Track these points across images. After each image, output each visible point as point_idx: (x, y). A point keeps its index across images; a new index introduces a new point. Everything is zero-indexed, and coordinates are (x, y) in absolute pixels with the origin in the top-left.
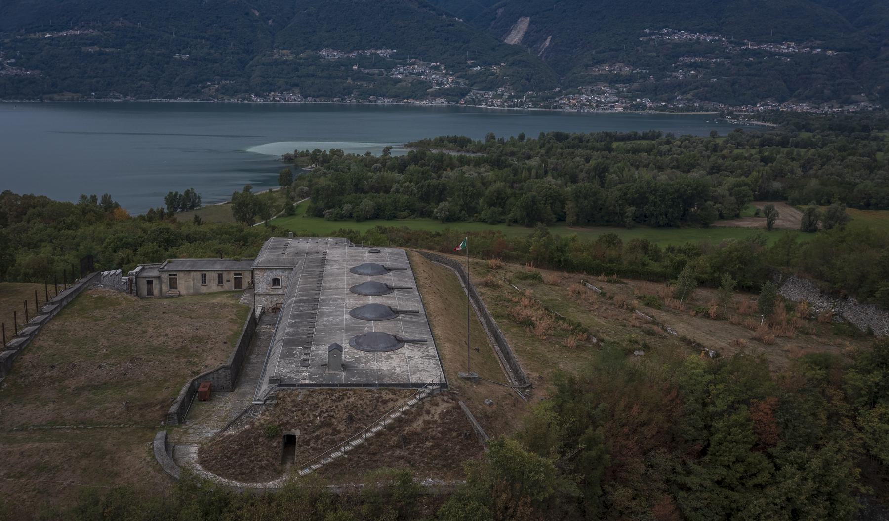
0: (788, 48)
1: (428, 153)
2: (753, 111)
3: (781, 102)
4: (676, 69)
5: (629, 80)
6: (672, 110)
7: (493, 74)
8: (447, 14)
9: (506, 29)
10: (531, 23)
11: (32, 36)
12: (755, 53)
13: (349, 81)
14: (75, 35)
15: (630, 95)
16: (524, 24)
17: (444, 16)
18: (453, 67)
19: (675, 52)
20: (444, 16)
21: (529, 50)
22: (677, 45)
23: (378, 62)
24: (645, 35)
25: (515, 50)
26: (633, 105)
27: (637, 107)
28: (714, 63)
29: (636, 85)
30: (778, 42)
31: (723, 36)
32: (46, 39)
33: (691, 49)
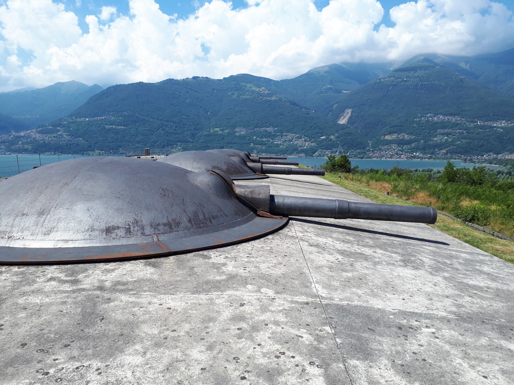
0: (501, 123)
1: (313, 339)
2: (482, 159)
3: (498, 154)
4: (436, 136)
5: (409, 142)
6: (435, 159)
7: (331, 140)
8: (306, 108)
9: (338, 117)
10: (352, 112)
11: (79, 120)
12: (481, 127)
13: (252, 145)
14: (102, 119)
15: (410, 151)
16: (348, 113)
17: (304, 109)
18: (311, 137)
19: (434, 127)
20: (304, 109)
21: (351, 127)
22: (436, 123)
23: (269, 135)
24: (418, 117)
25: (343, 127)
26: (412, 157)
27: (414, 157)
28: (458, 132)
29: (413, 145)
30: (496, 120)
31: (463, 118)
32: (86, 121)
33: (444, 125)
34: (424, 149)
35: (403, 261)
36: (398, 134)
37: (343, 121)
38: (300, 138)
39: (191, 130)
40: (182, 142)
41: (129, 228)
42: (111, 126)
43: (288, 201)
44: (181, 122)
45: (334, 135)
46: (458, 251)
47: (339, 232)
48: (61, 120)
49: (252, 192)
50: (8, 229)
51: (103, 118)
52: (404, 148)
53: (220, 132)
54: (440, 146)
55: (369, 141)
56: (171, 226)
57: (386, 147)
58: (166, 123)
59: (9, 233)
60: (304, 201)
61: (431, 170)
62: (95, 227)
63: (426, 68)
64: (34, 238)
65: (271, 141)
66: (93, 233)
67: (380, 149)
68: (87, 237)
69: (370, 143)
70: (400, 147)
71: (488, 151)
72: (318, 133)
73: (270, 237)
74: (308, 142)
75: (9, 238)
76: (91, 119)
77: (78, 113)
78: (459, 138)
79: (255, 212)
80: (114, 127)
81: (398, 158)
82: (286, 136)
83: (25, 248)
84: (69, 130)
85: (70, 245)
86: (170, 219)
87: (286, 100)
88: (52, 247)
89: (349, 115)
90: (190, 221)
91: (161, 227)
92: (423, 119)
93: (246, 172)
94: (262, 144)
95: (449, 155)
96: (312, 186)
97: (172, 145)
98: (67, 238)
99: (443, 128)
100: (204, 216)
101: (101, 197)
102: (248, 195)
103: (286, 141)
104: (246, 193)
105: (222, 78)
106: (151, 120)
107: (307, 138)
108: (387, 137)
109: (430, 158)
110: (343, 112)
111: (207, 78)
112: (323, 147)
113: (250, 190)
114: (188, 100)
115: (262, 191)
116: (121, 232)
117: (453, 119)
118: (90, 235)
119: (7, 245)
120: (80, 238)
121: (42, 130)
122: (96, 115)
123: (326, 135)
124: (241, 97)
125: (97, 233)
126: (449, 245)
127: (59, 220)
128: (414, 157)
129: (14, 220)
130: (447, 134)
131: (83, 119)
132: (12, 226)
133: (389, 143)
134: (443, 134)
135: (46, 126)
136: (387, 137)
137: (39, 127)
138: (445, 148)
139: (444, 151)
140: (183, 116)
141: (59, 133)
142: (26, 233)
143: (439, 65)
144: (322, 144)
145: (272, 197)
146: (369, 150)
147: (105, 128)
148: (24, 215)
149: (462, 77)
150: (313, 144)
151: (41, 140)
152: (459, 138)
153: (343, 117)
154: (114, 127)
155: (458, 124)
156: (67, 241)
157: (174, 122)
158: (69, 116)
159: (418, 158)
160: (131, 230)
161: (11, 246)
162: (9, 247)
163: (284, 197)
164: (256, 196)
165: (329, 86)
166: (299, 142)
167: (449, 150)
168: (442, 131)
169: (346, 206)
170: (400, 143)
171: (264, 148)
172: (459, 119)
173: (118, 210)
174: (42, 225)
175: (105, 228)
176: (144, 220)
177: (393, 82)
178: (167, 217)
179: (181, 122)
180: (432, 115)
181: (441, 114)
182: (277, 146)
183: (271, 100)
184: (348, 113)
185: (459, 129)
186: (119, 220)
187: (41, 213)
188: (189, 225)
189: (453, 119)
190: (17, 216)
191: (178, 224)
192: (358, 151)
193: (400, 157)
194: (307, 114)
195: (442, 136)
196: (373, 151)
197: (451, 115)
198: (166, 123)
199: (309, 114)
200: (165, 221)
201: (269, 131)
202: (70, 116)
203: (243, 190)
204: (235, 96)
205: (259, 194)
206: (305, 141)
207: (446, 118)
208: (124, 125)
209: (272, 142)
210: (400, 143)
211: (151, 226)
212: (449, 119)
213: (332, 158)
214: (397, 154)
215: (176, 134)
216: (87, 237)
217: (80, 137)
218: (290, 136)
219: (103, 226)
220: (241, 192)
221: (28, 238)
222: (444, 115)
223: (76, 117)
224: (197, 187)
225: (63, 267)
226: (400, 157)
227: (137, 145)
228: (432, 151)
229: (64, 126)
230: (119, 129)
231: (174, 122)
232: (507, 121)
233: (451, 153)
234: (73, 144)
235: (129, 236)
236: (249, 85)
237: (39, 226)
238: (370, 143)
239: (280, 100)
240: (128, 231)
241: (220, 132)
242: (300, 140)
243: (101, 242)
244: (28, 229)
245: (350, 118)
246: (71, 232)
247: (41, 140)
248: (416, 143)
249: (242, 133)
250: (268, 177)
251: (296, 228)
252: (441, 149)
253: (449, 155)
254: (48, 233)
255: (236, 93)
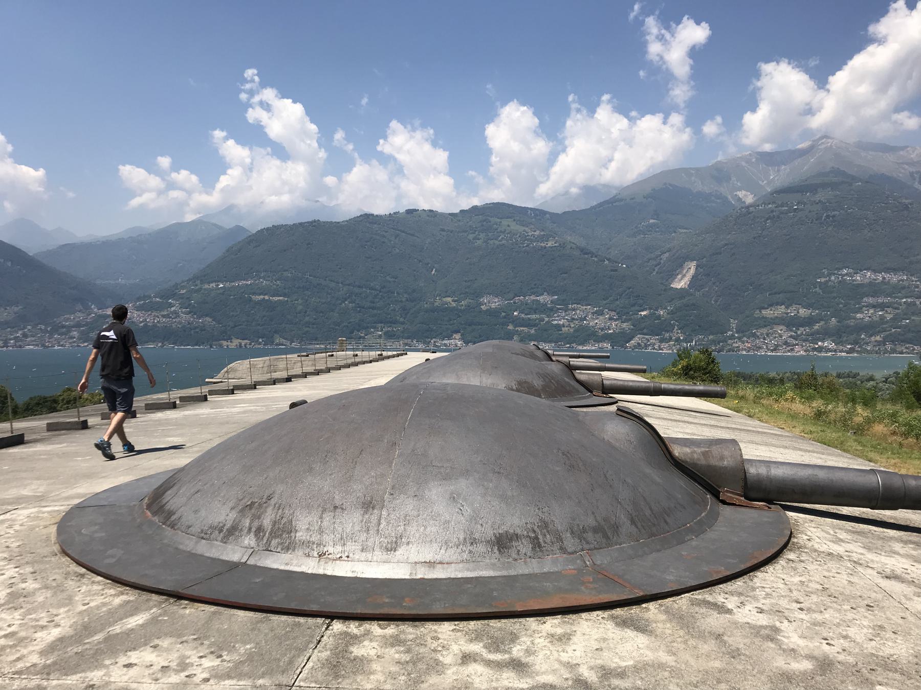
4: (860, 310)
7: (659, 317)
9: (672, 274)
10: (697, 267)
11: (206, 286)
13: (511, 327)
16: (691, 268)
18: (622, 315)
19: (857, 292)
20: (606, 262)
24: (823, 276)
25: (682, 293)
28: (905, 303)
29: (816, 327)
33: (874, 289)
34: (838, 335)
36: (787, 308)
37: (680, 284)
38: (600, 313)
39: (401, 301)
40: (384, 323)
41: (537, 538)
42: (262, 297)
44: (384, 287)
45: (666, 308)
48: (176, 286)
49: (705, 454)
50: (315, 538)
51: (249, 283)
52: (799, 332)
53: (454, 304)
54: (871, 328)
55: (732, 320)
56: (606, 533)
57: (764, 331)
58: (356, 290)
59: (319, 545)
60: (809, 472)
61: (855, 375)
62: (477, 536)
63: (833, 186)
64: (369, 556)
65: (547, 319)
66: (473, 548)
67: (754, 335)
68: (465, 556)
69: (734, 323)
70: (792, 331)
72: (634, 305)
74: (616, 320)
75: (320, 556)
76: (228, 284)
77: (205, 276)
78: (905, 314)
79: (716, 494)
80: (267, 297)
81: (789, 351)
82: (574, 310)
83: (356, 578)
84: (190, 305)
85: (439, 573)
86: (599, 519)
87: (574, 246)
88: (407, 577)
89: (692, 271)
90: (633, 522)
91: (590, 536)
92: (833, 278)
93: (578, 392)
94: (529, 324)
95: (889, 346)
97: (368, 327)
98: (429, 557)
99: (875, 294)
100: (651, 509)
101: (466, 473)
102: (698, 459)
103: (574, 319)
104: (695, 456)
105: (458, 211)
106: (333, 285)
107: (613, 313)
108: (768, 313)
110: (681, 266)
111: (431, 211)
112: (645, 331)
113: (703, 449)
114: (398, 251)
115: (726, 453)
116: (525, 547)
117: (894, 278)
118: (470, 552)
119: (321, 572)
120: (454, 558)
121: (144, 304)
122: (237, 278)
123: (650, 309)
124: (491, 242)
125: (481, 548)
127: (407, 521)
128: (820, 349)
129: (321, 518)
130: (882, 306)
131: (213, 285)
132: (321, 531)
133: (769, 323)
134: (874, 306)
135: (149, 297)
136: (768, 313)
137: (139, 299)
138: (879, 332)
139: (878, 338)
140: (388, 278)
141: (173, 309)
142: (350, 546)
143: (860, 180)
144: (643, 325)
146: (732, 337)
147: (250, 300)
148: (336, 507)
149: (907, 201)
150: (624, 325)
151: (141, 322)
152: (905, 314)
153: (679, 276)
154: (267, 297)
155: (904, 288)
156: (431, 564)
157: (372, 289)
158: (189, 280)
160: (541, 541)
161: (329, 573)
162: (325, 576)
163: (768, 463)
164: (714, 462)
165: (651, 221)
166: (596, 322)
167: (887, 336)
168: (871, 300)
170: (792, 323)
171: (533, 331)
172: (905, 278)
173: (503, 498)
174: (378, 530)
175: (493, 538)
176: (556, 521)
177: (772, 211)
178: (593, 513)
179: (384, 287)
180: (851, 271)
181: (868, 269)
182: (559, 327)
183: (545, 247)
185: (906, 297)
186: (515, 521)
187: (368, 505)
188: (633, 529)
190: (324, 510)
191: (616, 528)
192: (711, 337)
193: (792, 350)
194: (612, 270)
195: (871, 311)
196: (740, 338)
197: (888, 270)
198: (356, 290)
199: (616, 270)
200: (591, 521)
201: (542, 301)
202: (195, 279)
203: (688, 450)
205: (722, 458)
206: (611, 319)
207: (880, 277)
208: (285, 295)
209: (548, 322)
210: (792, 323)
211: (572, 533)
212: (884, 278)
213: (684, 354)
214: (786, 343)
215: (373, 308)
216: (465, 556)
217: (207, 316)
218: (580, 311)
219: (490, 534)
220: (685, 454)
221: (357, 557)
222: (875, 271)
223: (202, 282)
224: (609, 444)
225: (462, 624)
226: (792, 350)
227: (307, 329)
228: (853, 337)
229: (181, 297)
230: (276, 302)
231: (372, 289)
233: (893, 341)
234: (196, 328)
235: (540, 554)
236: (505, 222)
237: (371, 532)
238: (734, 323)
239: (563, 246)
240: (536, 545)
241: (454, 304)
242: (601, 318)
243: (493, 566)
244: (352, 538)
245: (694, 277)
246: (435, 546)
247: (141, 322)
248: (822, 323)
249: (493, 305)
252: (871, 336)
253: (889, 346)
254: (392, 548)
255: (482, 236)
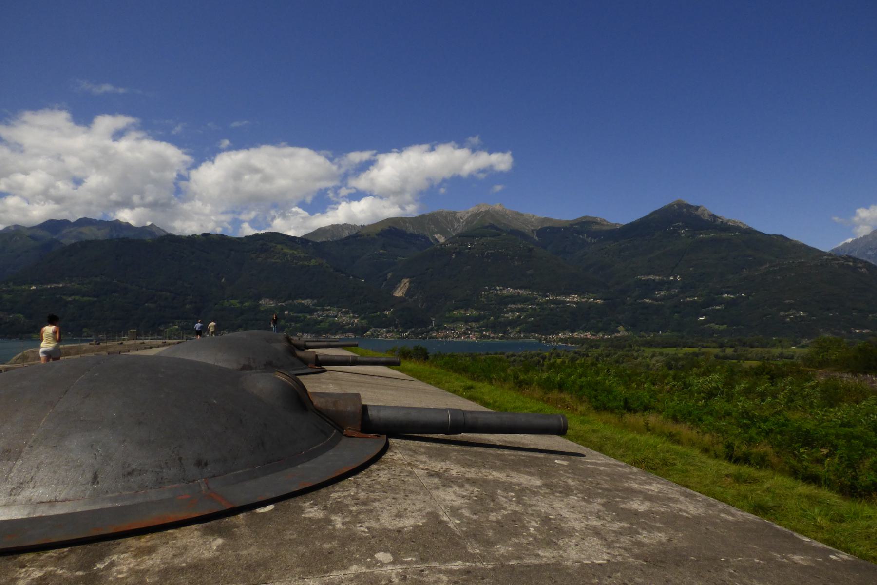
3: (573, 332)
5: (477, 319)
6: (507, 339)
9: (394, 288)
12: (553, 302)
16: (405, 283)
25: (401, 300)
30: (568, 294)
33: (514, 299)
35: (546, 485)
37: (399, 293)
38: (347, 313)
42: (73, 297)
43: (384, 415)
46: (596, 464)
47: (458, 451)
53: (238, 305)
54: (513, 323)
57: (451, 325)
71: (563, 329)
73: (374, 467)
85: (60, 510)
88: (25, 517)
94: (295, 320)
96: (380, 380)
109: (502, 338)
126: (583, 456)
130: (519, 310)
145: (365, 408)
159: (489, 337)
169: (460, 417)
184: (405, 283)
189: (524, 293)
197: (521, 288)
203: (322, 400)
204: (260, 259)
232: (579, 296)
236: (279, 246)
241: (238, 305)
250: (326, 371)
251: (400, 451)
